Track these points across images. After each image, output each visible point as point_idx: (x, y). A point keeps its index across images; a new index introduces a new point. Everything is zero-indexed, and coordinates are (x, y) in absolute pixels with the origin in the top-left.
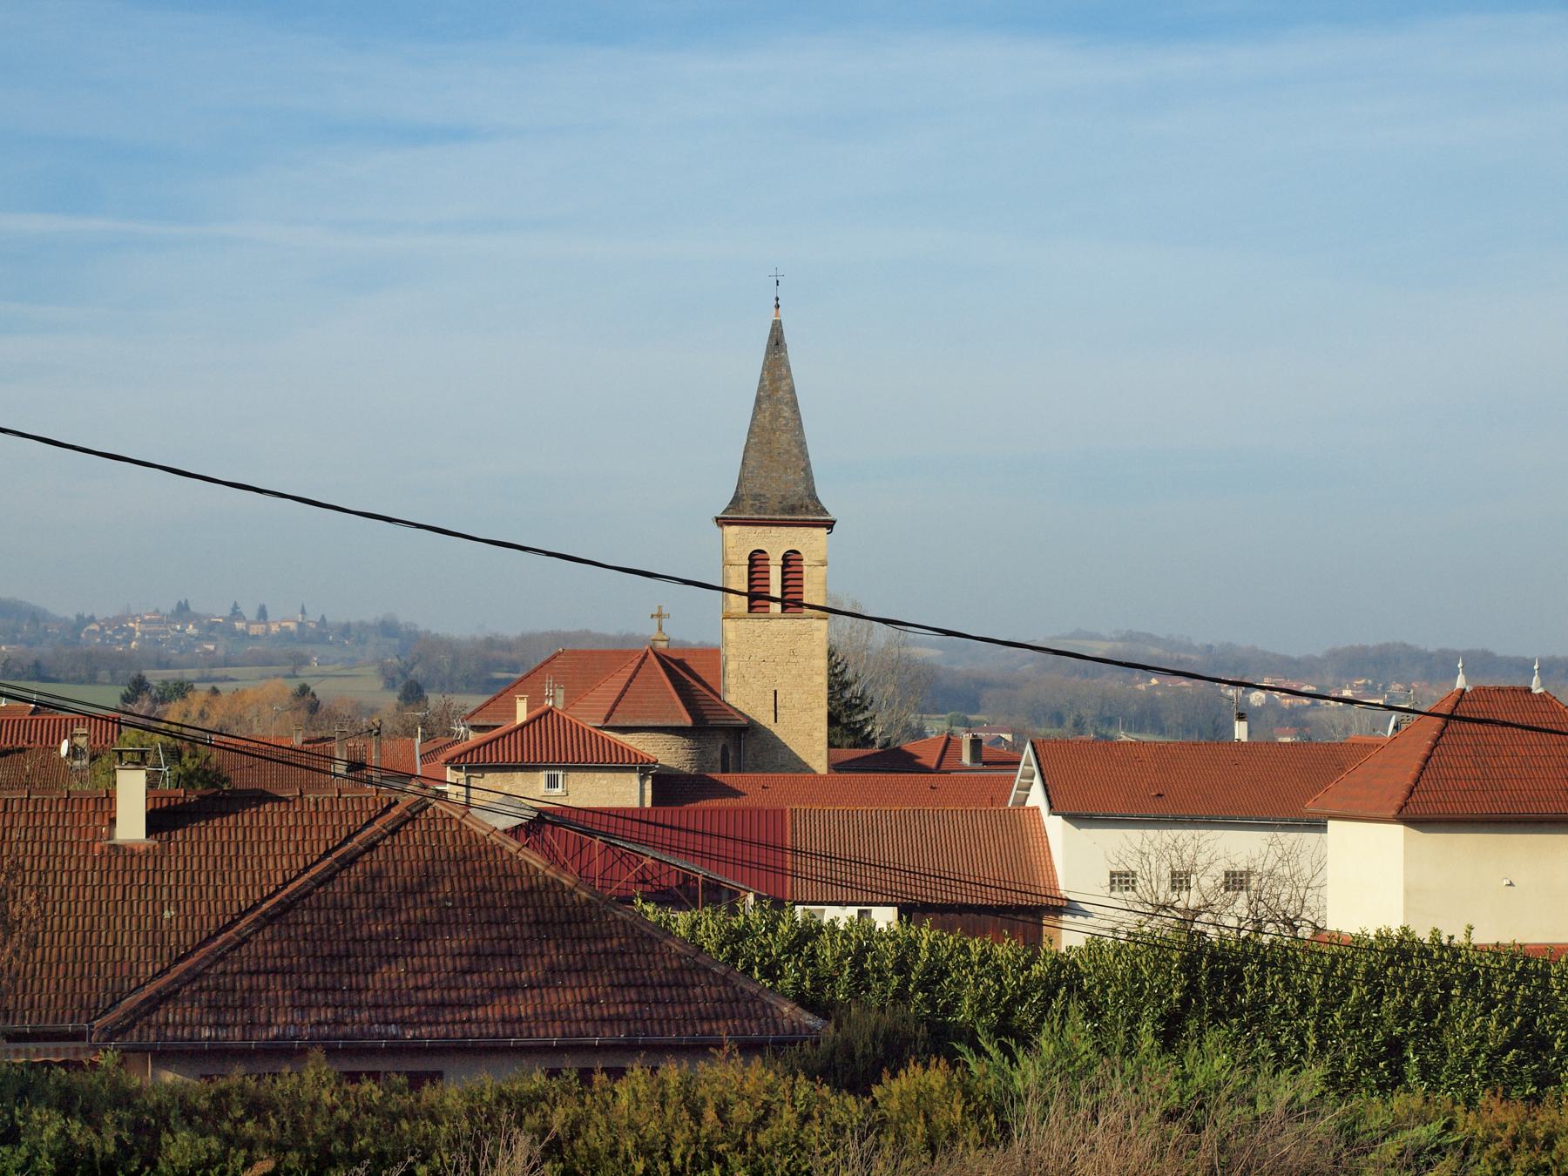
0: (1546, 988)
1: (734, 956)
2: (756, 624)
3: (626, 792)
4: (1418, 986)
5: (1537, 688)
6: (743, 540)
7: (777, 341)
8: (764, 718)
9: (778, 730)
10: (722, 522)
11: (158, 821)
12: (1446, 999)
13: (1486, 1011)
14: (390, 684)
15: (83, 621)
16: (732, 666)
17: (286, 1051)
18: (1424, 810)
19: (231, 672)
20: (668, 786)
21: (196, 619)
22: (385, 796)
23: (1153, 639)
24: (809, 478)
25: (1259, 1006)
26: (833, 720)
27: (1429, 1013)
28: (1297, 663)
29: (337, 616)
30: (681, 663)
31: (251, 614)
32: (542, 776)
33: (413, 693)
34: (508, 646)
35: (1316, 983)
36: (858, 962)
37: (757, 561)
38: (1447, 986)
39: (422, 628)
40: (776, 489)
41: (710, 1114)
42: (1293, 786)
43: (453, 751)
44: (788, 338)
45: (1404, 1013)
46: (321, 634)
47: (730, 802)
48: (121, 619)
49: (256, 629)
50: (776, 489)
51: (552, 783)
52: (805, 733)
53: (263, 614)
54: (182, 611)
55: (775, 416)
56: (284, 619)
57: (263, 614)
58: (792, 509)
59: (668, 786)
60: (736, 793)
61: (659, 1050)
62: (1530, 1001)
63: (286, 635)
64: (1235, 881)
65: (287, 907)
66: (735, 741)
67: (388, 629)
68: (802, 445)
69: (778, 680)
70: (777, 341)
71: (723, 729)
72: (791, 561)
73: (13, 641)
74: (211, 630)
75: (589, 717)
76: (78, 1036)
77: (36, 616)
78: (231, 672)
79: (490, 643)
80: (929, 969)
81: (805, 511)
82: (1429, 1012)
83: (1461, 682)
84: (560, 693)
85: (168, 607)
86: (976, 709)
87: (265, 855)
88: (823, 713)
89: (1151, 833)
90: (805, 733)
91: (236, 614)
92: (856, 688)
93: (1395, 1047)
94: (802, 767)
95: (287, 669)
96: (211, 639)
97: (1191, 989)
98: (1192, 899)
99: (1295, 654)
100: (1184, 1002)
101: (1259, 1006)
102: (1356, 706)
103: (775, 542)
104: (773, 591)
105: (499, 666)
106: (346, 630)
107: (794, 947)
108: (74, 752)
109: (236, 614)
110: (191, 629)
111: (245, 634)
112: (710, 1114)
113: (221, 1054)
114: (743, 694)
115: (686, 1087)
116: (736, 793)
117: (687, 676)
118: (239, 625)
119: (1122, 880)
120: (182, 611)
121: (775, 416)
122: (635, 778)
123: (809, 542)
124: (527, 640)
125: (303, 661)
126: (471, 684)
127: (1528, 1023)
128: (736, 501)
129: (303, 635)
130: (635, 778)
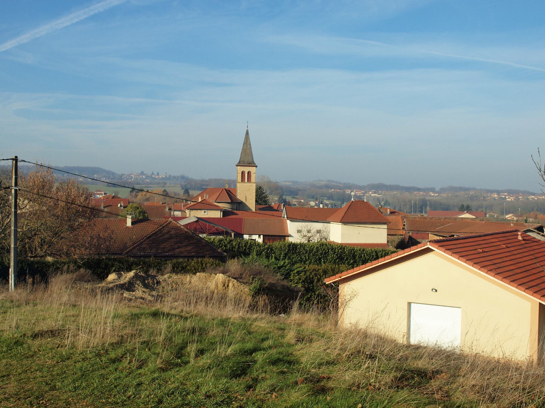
0: (344, 250)
1: (220, 244)
2: (243, 184)
3: (217, 214)
4: (324, 250)
5: (365, 201)
6: (240, 169)
7: (247, 133)
8: (244, 201)
9: (246, 203)
10: (237, 166)
11: (133, 223)
12: (328, 251)
13: (334, 254)
14: (183, 188)
15: (123, 175)
16: (238, 191)
17: (149, 257)
18: (345, 221)
19: (151, 186)
20: (226, 213)
21: (145, 175)
22: (166, 220)
23: (334, 182)
24: (253, 158)
25: (299, 252)
26: (256, 201)
27: (325, 254)
28: (360, 186)
29: (173, 174)
30: (229, 191)
31: (156, 174)
32: (203, 211)
33: (187, 191)
34: (206, 181)
35: (308, 249)
36: (239, 245)
37: (243, 173)
38: (329, 250)
39: (189, 177)
40: (247, 160)
41: (204, 265)
42: (323, 216)
43: (188, 206)
44: (249, 133)
45: (321, 254)
46: (169, 178)
47: (233, 216)
48: (130, 175)
49: (157, 177)
50: (247, 160)
51: (205, 212)
52: (251, 203)
53: (158, 174)
54: (142, 173)
55: (247, 147)
56: (162, 175)
57: (158, 174)
58: (250, 164)
59: (226, 213)
60: (237, 214)
61: (198, 257)
62: (341, 252)
63: (162, 178)
64: (319, 232)
65: (150, 237)
66: (239, 205)
67: (183, 177)
68: (251, 152)
69: (246, 194)
70: (247, 133)
71: (237, 203)
72: (249, 173)
73: (109, 179)
74: (148, 177)
75: (212, 201)
76: (121, 254)
77: (113, 174)
78: (151, 186)
79: (202, 181)
80: (249, 246)
81: (252, 164)
82: (325, 253)
83: (352, 200)
84: (207, 196)
85: (140, 172)
86: (297, 195)
87: (148, 229)
88: (254, 200)
89: (303, 223)
90: (251, 203)
91: (153, 174)
92: (266, 194)
93: (320, 259)
94: (251, 210)
95: (162, 185)
96: (148, 179)
97: (289, 250)
98: (310, 235)
99: (361, 185)
100: (288, 252)
101: (299, 252)
102: (213, 230)
103: (246, 169)
104: (246, 177)
105: (204, 185)
106: (174, 177)
107: (229, 243)
108: (121, 206)
109: (153, 174)
110: (144, 177)
111: (155, 178)
112: (204, 265)
113: (141, 256)
114: (240, 196)
115: (201, 261)
116: (237, 214)
117: (231, 194)
118: (153, 176)
119: (299, 231)
120: (142, 173)
121: (247, 147)
122: (219, 211)
123: (253, 170)
124: (210, 180)
125: (165, 184)
126: (198, 189)
127: (341, 255)
128: (240, 162)
129: (166, 178)
130: (219, 211)
